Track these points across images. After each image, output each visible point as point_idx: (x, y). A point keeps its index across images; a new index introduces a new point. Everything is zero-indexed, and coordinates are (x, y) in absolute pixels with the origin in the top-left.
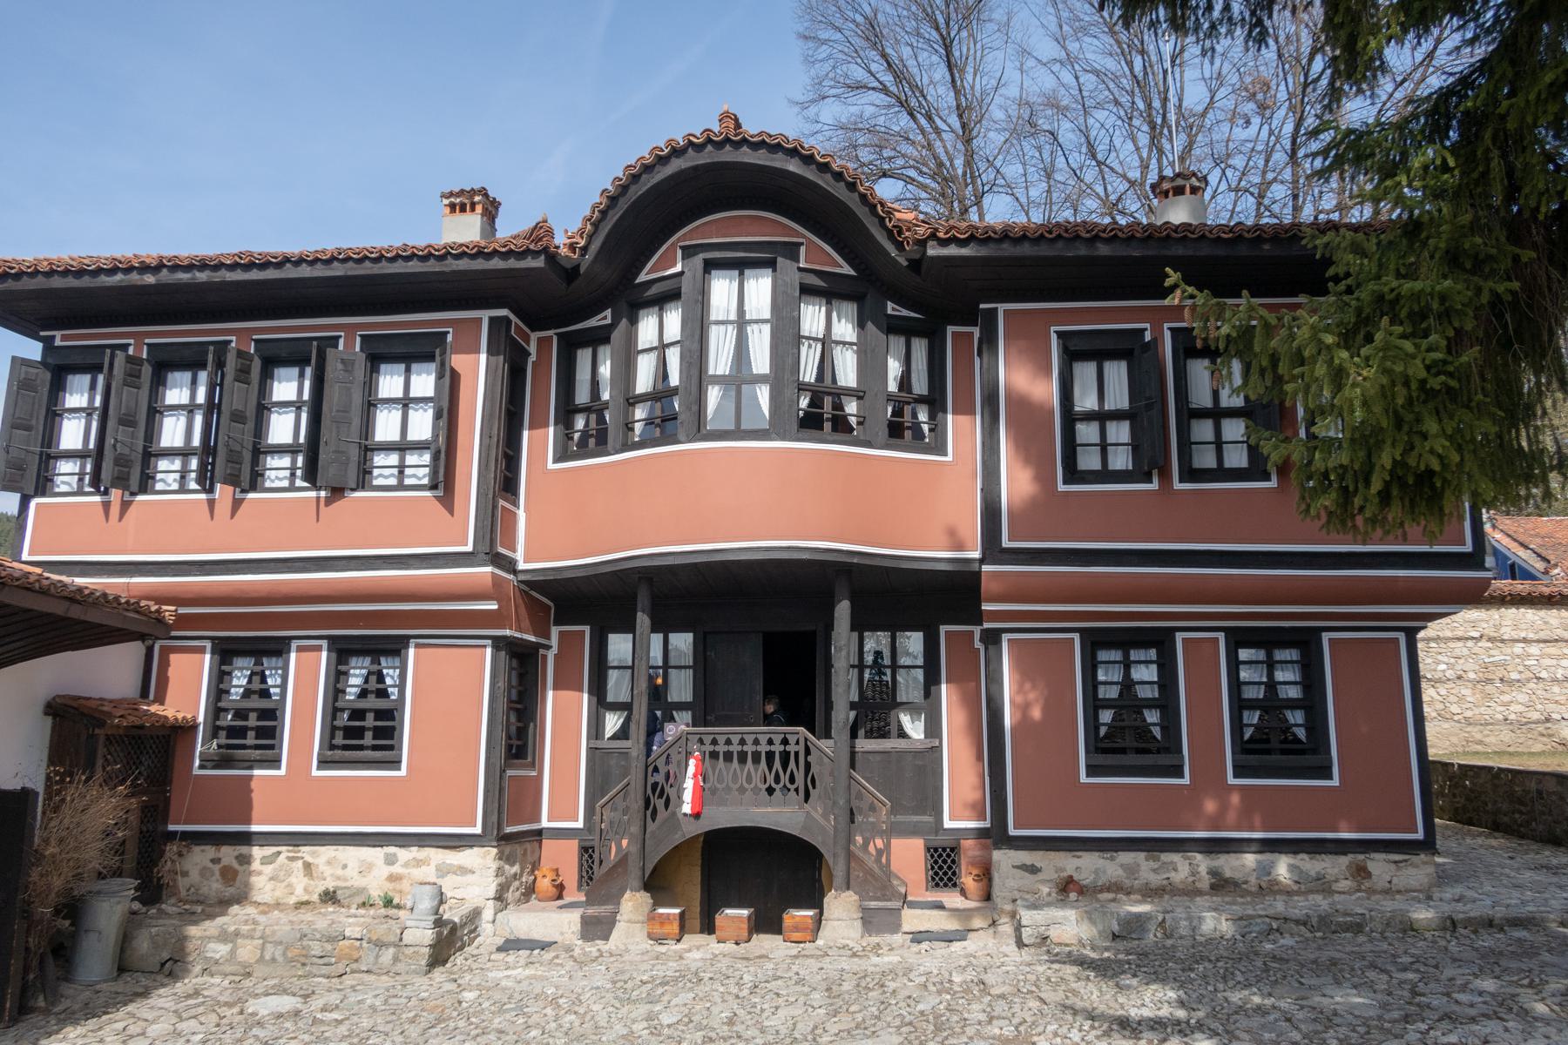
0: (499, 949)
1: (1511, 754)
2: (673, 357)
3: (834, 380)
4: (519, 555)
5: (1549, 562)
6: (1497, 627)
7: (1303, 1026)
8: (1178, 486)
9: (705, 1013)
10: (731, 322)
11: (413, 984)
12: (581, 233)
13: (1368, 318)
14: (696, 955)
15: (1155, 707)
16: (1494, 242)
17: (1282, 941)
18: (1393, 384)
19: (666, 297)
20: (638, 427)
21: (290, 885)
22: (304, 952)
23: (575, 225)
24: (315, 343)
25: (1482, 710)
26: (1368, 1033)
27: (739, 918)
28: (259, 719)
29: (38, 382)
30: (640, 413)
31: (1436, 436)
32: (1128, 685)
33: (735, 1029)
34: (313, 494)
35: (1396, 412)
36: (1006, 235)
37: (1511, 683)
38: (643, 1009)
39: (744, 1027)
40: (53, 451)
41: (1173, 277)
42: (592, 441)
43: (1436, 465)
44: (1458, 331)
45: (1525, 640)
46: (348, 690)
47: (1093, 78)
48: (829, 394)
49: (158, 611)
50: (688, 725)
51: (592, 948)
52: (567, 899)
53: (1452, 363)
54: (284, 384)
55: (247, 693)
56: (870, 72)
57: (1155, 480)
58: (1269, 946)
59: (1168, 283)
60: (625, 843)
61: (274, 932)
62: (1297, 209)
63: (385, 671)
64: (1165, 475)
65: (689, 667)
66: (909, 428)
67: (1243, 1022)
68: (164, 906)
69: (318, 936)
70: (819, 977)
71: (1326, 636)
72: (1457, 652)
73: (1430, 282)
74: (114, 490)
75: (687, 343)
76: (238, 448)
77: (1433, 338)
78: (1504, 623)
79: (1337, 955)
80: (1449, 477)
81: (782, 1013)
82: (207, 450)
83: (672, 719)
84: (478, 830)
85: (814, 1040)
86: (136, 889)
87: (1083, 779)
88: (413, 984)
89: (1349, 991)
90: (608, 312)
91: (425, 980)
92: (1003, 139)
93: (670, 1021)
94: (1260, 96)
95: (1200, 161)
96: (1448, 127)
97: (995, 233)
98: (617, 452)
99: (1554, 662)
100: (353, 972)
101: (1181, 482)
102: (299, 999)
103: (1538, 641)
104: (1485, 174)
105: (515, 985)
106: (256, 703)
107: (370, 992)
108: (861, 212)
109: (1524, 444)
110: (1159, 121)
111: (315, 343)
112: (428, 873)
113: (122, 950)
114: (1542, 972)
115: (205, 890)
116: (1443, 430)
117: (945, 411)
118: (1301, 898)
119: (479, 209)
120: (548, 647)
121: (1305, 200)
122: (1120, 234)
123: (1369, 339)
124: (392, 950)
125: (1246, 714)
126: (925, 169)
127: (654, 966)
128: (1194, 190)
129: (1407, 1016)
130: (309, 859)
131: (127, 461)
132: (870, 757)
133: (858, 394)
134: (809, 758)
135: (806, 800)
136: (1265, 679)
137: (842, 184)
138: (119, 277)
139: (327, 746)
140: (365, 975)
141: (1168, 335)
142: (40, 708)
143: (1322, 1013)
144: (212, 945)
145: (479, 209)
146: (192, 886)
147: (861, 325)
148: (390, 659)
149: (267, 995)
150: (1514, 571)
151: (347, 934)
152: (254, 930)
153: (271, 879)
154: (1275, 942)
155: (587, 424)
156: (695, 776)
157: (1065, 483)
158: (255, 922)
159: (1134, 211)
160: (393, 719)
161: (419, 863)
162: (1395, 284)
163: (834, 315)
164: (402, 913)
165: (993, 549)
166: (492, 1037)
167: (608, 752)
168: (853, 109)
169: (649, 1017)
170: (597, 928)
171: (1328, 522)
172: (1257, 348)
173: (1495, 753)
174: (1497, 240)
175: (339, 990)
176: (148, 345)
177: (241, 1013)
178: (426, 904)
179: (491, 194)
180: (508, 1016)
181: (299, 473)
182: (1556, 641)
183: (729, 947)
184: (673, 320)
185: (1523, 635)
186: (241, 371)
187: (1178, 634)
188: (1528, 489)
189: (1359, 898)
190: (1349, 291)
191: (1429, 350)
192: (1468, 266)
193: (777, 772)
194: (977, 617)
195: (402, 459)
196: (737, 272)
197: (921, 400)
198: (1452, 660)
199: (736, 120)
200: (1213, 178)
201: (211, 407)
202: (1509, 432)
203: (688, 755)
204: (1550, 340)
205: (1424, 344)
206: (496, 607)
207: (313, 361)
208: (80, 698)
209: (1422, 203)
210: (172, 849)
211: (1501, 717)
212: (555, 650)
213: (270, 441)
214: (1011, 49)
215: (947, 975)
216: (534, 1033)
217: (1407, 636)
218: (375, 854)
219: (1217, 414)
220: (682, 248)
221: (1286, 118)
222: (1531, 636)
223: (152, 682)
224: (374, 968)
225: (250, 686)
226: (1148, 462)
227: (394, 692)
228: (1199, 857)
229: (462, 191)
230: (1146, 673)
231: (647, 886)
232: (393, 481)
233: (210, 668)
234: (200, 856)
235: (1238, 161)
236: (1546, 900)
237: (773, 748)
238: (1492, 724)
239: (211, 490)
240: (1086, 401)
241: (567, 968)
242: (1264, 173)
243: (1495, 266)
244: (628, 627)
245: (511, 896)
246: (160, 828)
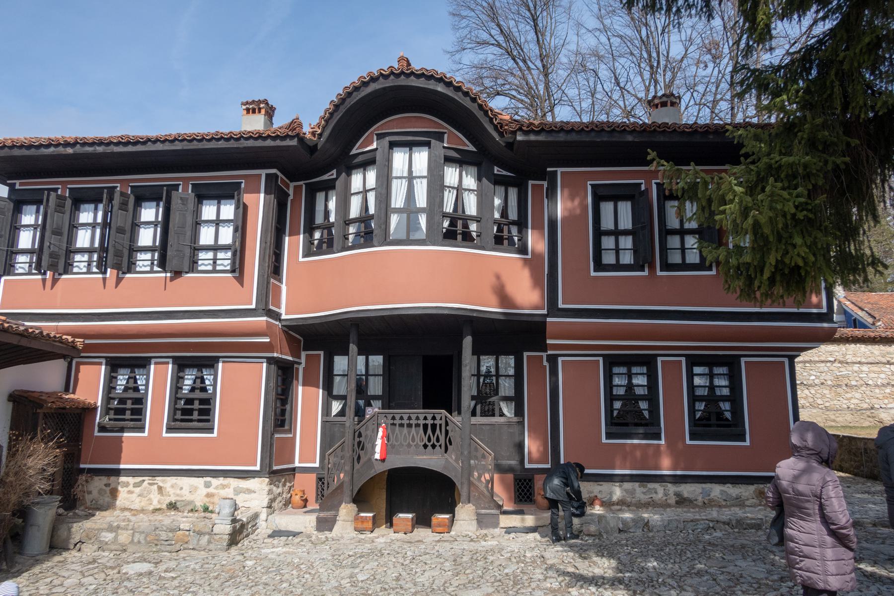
0: (270, 536)
1: (851, 427)
2: (371, 198)
3: (464, 211)
4: (283, 310)
5: (875, 318)
6: (844, 355)
7: (722, 584)
8: (659, 273)
9: (383, 574)
10: (404, 178)
11: (218, 556)
12: (319, 125)
13: (763, 178)
14: (382, 540)
15: (645, 400)
16: (835, 134)
17: (715, 534)
18: (777, 216)
19: (368, 163)
20: (351, 237)
21: (150, 499)
22: (157, 538)
23: (315, 121)
24: (165, 188)
25: (835, 402)
26: (759, 588)
27: (407, 519)
28: (133, 404)
29: (6, 209)
30: (352, 229)
31: (801, 246)
32: (630, 387)
33: (400, 583)
34: (163, 275)
35: (778, 232)
36: (564, 128)
37: (851, 387)
38: (348, 572)
39: (404, 582)
40: (72, 248)
41: (652, 154)
42: (325, 246)
43: (801, 263)
44: (815, 186)
45: (860, 363)
46: (184, 387)
47: (619, 40)
48: (460, 219)
49: (73, 342)
50: (379, 409)
51: (322, 536)
52: (309, 508)
53: (811, 204)
54: (148, 210)
55: (126, 389)
56: (490, 35)
57: (647, 270)
58: (707, 537)
59: (649, 158)
60: (342, 475)
61: (139, 526)
62: (733, 116)
63: (205, 377)
64: (652, 267)
65: (380, 375)
66: (506, 239)
67: (689, 581)
68: (77, 511)
69: (165, 529)
70: (450, 553)
71: (743, 360)
72: (822, 369)
73: (799, 157)
74: (48, 272)
75: (379, 190)
76: (121, 248)
77: (800, 189)
78: (848, 353)
79: (745, 542)
80: (808, 269)
81: (427, 574)
82: (103, 249)
83: (370, 405)
84: (258, 468)
85: (444, 590)
86: (60, 501)
87: (604, 440)
88: (218, 556)
89: (750, 563)
90: (334, 171)
91: (226, 554)
92: (566, 74)
93: (363, 579)
94: (713, 51)
95: (679, 88)
96: (811, 68)
97: (556, 127)
98: (339, 252)
99: (876, 375)
100: (185, 549)
101: (661, 271)
102: (152, 565)
103: (867, 363)
104: (830, 96)
105: (277, 557)
106: (131, 394)
107: (193, 561)
108: (479, 114)
109: (853, 251)
110: (655, 65)
111: (165, 188)
112: (229, 493)
113: (52, 536)
114: (861, 553)
115: (101, 502)
116: (805, 242)
117: (527, 227)
118: (727, 509)
119: (263, 111)
120: (300, 363)
121: (738, 110)
122: (627, 129)
123: (763, 190)
124: (207, 537)
125: (697, 404)
126: (521, 91)
127: (357, 546)
128: (673, 104)
129: (782, 578)
130: (161, 484)
131: (57, 255)
132: (484, 427)
133: (477, 220)
134: (448, 428)
135: (446, 452)
136: (708, 384)
137: (468, 98)
138: (52, 149)
139: (171, 419)
140: (192, 551)
141: (654, 187)
142: (5, 397)
143: (734, 576)
144: (104, 534)
145: (263, 111)
146: (94, 499)
147: (479, 179)
148: (208, 370)
149: (134, 562)
150: (855, 323)
151: (181, 527)
152: (128, 525)
153: (139, 495)
154: (711, 534)
155: (322, 236)
156: (382, 437)
157: (595, 271)
158: (129, 521)
159: (643, 116)
160: (142, 404)
161: (224, 487)
162: (778, 158)
163: (464, 173)
164: (213, 516)
165: (553, 309)
166: (261, 587)
167: (333, 423)
168: (481, 56)
169: (351, 577)
170: (325, 524)
171: (741, 295)
172: (700, 196)
173: (842, 427)
174: (837, 133)
175: (176, 560)
176: (69, 188)
177: (119, 573)
178: (227, 511)
179: (270, 103)
180: (271, 575)
181: (156, 262)
182: (878, 363)
183: (401, 535)
184: (371, 176)
185: (859, 359)
186: (123, 204)
187: (742, 359)
188: (854, 276)
189: (760, 510)
190: (753, 163)
191: (797, 196)
192: (820, 148)
193: (429, 436)
194: (544, 348)
195: (215, 255)
196: (408, 149)
197: (514, 223)
198: (819, 374)
199: (408, 61)
200: (686, 98)
201: (105, 225)
202: (844, 244)
203: (378, 426)
204: (867, 192)
205: (795, 192)
206: (268, 340)
207: (164, 198)
208: (29, 391)
209: (796, 111)
210: (82, 478)
211: (846, 406)
212: (303, 365)
213: (139, 244)
214: (571, 23)
215: (523, 552)
216: (285, 585)
217: (789, 361)
218: (199, 482)
219: (682, 232)
220: (376, 134)
221: (728, 63)
222: (863, 360)
223: (69, 383)
224: (197, 547)
225: (127, 385)
226: (642, 260)
227: (210, 389)
228: (669, 485)
229: (253, 101)
230: (640, 381)
231: (355, 501)
232: (210, 268)
233: (105, 375)
234: (98, 483)
235: (701, 88)
236: (866, 511)
237: (427, 422)
238: (840, 410)
239: (105, 272)
240: (607, 223)
241: (307, 547)
242: (715, 94)
243: (836, 148)
244: (345, 352)
245: (275, 505)
246: (75, 466)
